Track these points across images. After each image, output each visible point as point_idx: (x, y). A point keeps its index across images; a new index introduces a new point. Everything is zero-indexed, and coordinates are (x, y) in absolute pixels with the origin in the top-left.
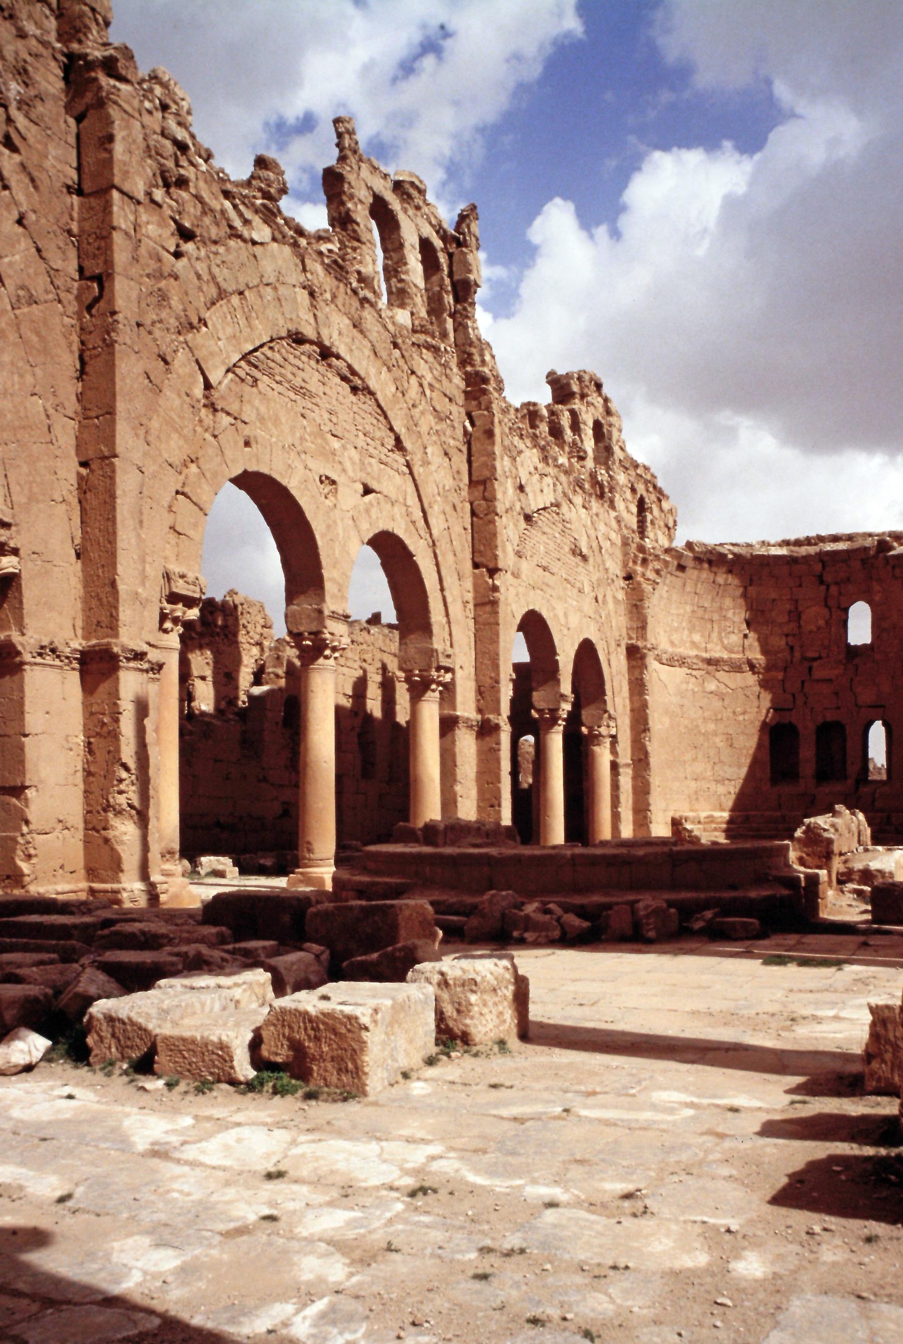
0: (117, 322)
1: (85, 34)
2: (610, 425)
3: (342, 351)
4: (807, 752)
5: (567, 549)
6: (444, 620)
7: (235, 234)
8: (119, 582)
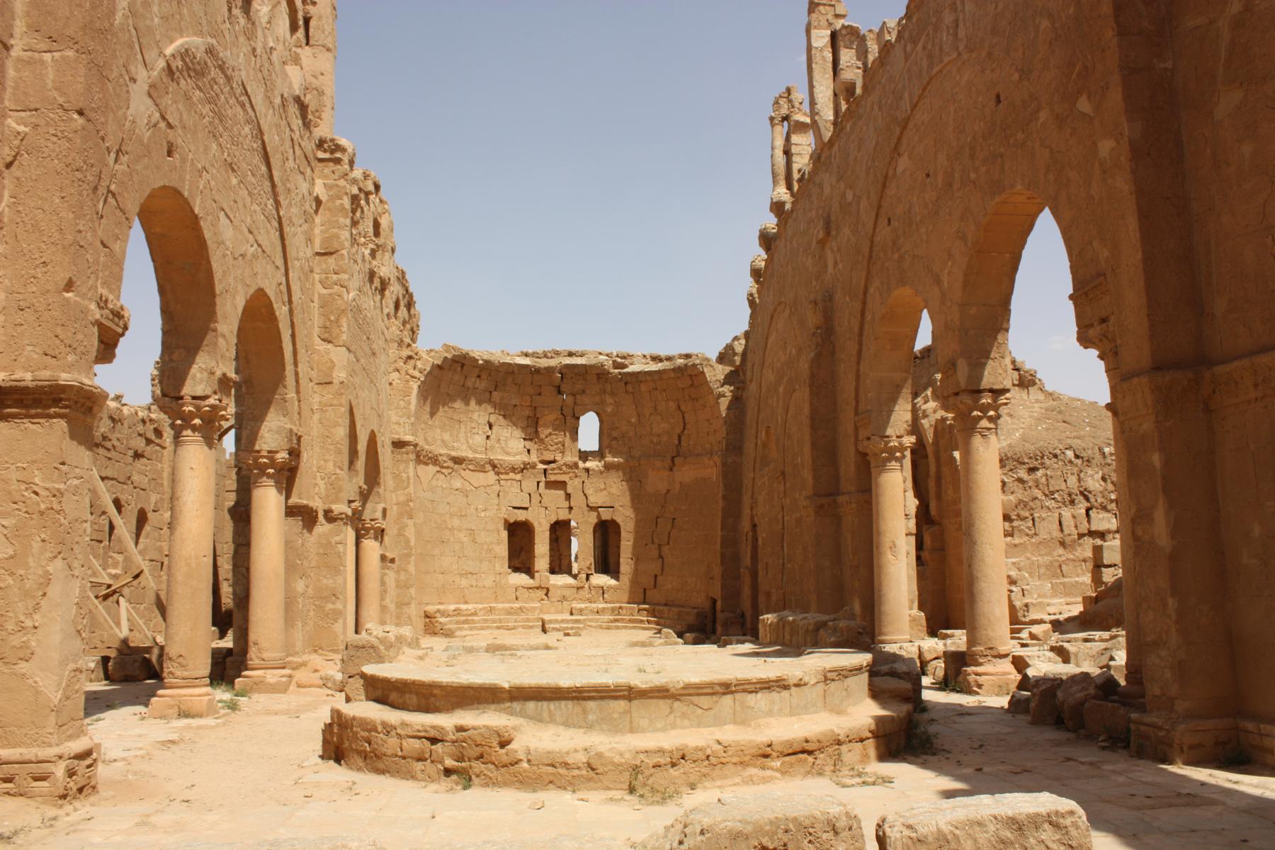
4: (542, 547)
6: (228, 221)
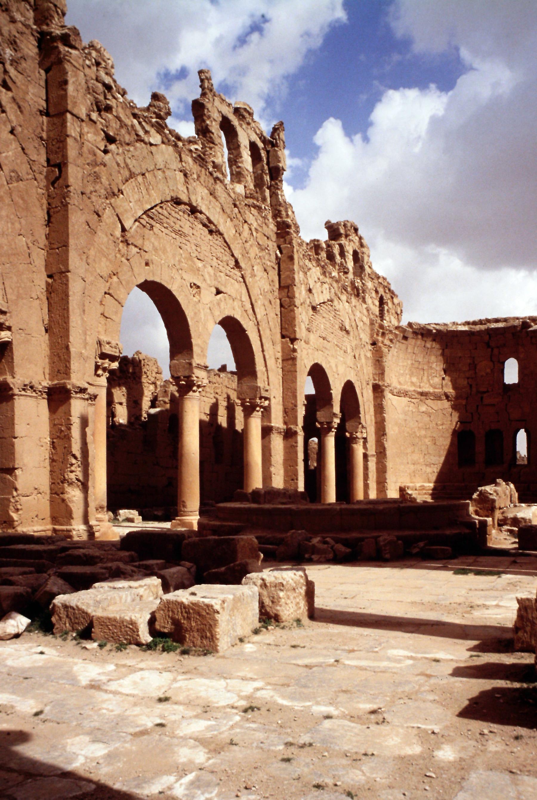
0: (70, 192)
1: (51, 21)
2: (363, 253)
3: (204, 209)
5: (337, 327)
7: (140, 140)
8: (71, 346)
